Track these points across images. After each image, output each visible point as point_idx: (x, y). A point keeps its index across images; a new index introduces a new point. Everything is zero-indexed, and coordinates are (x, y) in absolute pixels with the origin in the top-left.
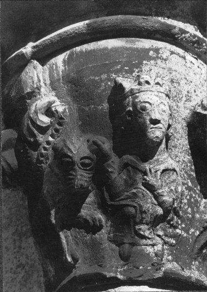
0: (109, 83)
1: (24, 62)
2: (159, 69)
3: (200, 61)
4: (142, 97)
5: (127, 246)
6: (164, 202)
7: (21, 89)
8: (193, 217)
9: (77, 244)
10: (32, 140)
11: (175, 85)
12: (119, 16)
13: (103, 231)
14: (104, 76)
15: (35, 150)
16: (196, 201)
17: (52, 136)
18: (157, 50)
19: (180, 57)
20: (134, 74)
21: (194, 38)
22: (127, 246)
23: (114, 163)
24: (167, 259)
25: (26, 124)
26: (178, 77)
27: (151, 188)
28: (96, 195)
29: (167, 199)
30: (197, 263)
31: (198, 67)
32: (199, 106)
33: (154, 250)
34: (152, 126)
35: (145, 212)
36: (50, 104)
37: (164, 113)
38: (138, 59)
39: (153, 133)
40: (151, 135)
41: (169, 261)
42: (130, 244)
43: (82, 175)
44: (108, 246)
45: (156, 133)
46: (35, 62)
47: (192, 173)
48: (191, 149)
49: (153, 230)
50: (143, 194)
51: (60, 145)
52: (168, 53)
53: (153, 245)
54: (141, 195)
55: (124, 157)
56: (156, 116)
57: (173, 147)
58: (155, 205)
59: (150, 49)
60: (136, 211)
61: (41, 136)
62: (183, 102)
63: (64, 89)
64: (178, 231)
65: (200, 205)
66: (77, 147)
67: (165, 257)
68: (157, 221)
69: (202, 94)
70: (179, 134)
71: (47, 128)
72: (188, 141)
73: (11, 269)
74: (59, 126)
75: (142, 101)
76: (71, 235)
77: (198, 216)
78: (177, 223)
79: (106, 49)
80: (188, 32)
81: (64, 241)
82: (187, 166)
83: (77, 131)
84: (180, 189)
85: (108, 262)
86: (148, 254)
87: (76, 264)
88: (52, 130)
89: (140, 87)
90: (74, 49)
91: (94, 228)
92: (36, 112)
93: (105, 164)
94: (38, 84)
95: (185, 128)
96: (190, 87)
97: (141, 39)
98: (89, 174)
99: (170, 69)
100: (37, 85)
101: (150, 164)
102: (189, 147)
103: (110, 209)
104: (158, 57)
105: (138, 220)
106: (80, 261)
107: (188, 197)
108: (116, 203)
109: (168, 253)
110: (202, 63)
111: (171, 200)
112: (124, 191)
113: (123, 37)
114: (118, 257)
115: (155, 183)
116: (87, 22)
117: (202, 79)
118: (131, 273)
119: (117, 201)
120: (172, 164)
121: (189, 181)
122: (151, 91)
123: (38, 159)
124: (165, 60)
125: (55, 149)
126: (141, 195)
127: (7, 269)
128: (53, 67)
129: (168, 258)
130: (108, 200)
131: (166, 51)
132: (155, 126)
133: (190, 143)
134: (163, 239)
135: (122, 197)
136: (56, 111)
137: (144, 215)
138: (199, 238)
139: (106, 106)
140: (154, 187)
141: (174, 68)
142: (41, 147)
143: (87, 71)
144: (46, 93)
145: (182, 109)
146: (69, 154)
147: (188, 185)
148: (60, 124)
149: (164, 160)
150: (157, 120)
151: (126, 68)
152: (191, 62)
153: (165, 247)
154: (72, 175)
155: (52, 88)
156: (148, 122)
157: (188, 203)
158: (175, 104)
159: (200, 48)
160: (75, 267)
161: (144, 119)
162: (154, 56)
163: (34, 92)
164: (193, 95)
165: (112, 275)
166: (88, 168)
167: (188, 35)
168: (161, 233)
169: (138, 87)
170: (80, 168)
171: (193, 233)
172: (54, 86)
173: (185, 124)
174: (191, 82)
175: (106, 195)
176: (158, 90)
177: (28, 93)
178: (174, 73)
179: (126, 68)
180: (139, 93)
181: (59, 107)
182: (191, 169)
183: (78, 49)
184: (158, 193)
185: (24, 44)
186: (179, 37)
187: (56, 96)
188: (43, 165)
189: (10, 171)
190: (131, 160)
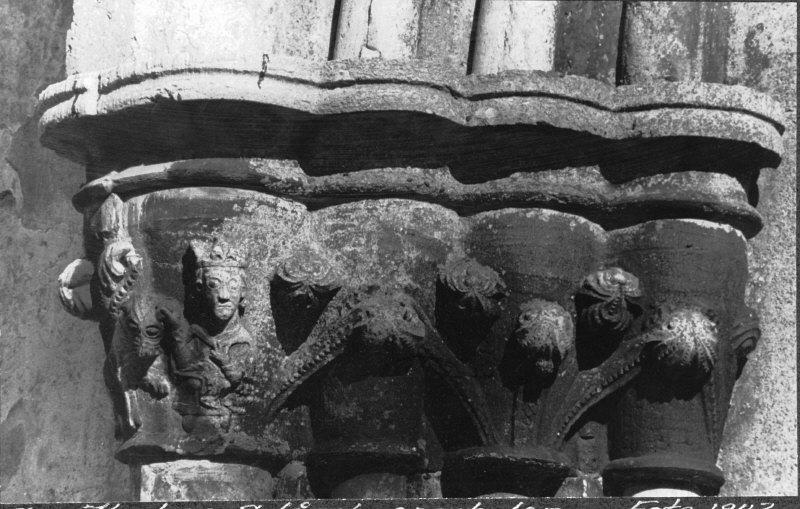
1: (102, 195)
7: (100, 225)
9: (141, 406)
13: (168, 397)
14: (181, 233)
15: (109, 296)
17: (125, 287)
18: (242, 203)
22: (191, 417)
23: (184, 329)
27: (219, 363)
36: (126, 252)
38: (212, 219)
44: (173, 415)
45: (224, 311)
46: (116, 197)
53: (219, 416)
56: (225, 294)
59: (234, 202)
63: (141, 237)
64: (250, 398)
67: (232, 427)
68: (222, 393)
71: (121, 277)
79: (187, 199)
81: (128, 401)
91: (158, 393)
97: (228, 189)
101: (218, 338)
104: (242, 212)
111: (240, 373)
113: (202, 185)
116: (168, 165)
118: (462, 64)
123: (110, 308)
124: (251, 214)
133: (272, 304)
135: (188, 369)
137: (210, 388)
148: (133, 277)
149: (240, 332)
153: (233, 416)
156: (216, 300)
161: (213, 296)
165: (172, 448)
167: (279, 184)
168: (228, 403)
173: (267, 283)
175: (173, 362)
181: (134, 258)
183: (159, 193)
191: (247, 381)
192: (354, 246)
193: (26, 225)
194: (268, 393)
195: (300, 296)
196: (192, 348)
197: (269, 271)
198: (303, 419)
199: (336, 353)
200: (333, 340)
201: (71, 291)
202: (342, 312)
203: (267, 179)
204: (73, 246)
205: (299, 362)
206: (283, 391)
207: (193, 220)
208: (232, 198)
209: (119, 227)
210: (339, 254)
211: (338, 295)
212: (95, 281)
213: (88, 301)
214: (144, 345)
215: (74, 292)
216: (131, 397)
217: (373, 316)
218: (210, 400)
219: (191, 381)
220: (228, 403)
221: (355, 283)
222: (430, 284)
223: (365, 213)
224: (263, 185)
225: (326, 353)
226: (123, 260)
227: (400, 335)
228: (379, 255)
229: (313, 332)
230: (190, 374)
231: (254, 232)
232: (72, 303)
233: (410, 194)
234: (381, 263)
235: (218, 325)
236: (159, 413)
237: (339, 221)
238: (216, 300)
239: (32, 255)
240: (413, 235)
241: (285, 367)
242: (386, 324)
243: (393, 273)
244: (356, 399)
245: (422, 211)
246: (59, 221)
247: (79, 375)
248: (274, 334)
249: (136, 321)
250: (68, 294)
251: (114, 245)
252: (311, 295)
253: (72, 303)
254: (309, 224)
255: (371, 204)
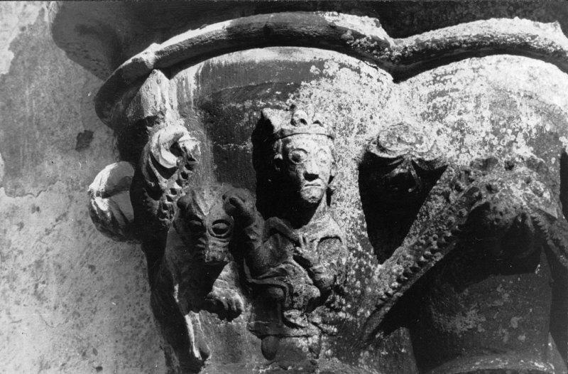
0: (255, 114)
1: (142, 73)
2: (323, 92)
3: (381, 71)
4: (296, 142)
5: (272, 339)
6: (321, 281)
7: (140, 111)
8: (363, 292)
9: (207, 333)
10: (153, 184)
11: (344, 112)
12: (272, 15)
13: (242, 316)
14: (248, 104)
15: (157, 199)
16: (369, 270)
17: (179, 182)
18: (320, 64)
19: (352, 70)
20: (288, 102)
21: (372, 43)
22: (272, 339)
23: (258, 226)
24: (325, 354)
25: (145, 162)
26: (348, 101)
27: (305, 263)
28: (233, 269)
29: (326, 276)
30: (367, 353)
31: (378, 80)
32: (374, 143)
33: (308, 343)
34: (307, 182)
35: (296, 295)
36: (178, 136)
37: (323, 164)
38: (288, 83)
39: (308, 193)
40: (306, 195)
41: (327, 357)
42: (275, 336)
43: (214, 244)
44: (248, 337)
45: (312, 191)
47: (363, 233)
48: (362, 199)
49: (308, 316)
50: (294, 271)
51: (188, 200)
52: (336, 66)
53: (307, 337)
54: (291, 271)
55: (272, 219)
56: (312, 169)
57: (338, 200)
58: (310, 284)
59: (311, 64)
60: (285, 293)
61: (164, 180)
62: (354, 135)
63: (197, 116)
64: (341, 315)
65: (373, 274)
66: (209, 206)
67: (323, 351)
68: (310, 305)
69: (381, 119)
70: (348, 180)
71: (173, 170)
72: (358, 190)
73: (132, 319)
74: (189, 169)
75: (295, 148)
76: (201, 320)
77: (369, 290)
78: (340, 304)
79: (252, 63)
80: (364, 36)
82: (357, 224)
83: (210, 179)
84: (344, 261)
85: (247, 360)
86: (300, 349)
87: (205, 360)
88: (179, 175)
89: (293, 127)
90: (211, 60)
91: (229, 312)
92: (158, 147)
93: (246, 229)
94: (162, 107)
95: (355, 171)
96: (365, 112)
97: (301, 48)
98: (225, 242)
99: (338, 91)
100: (160, 108)
101: (305, 231)
102: (359, 197)
103: (251, 289)
104: (321, 75)
105: (287, 305)
106: (210, 357)
107: (357, 267)
108: (261, 282)
109: (326, 346)
110: (384, 72)
111: (332, 277)
112: (269, 266)
114: (261, 354)
115: (310, 257)
116: (227, 23)
117: (382, 97)
119: (260, 279)
120: (333, 230)
121: (359, 244)
122: (307, 133)
123: (159, 211)
124: (332, 78)
125: (181, 205)
126: (291, 271)
127: (127, 320)
128: (182, 84)
129: (326, 353)
130: (249, 276)
131: (333, 63)
132: (311, 183)
134: (320, 328)
135: (267, 275)
136: (185, 148)
137: (295, 299)
138: (371, 321)
139: (249, 145)
140: (309, 262)
141: (343, 89)
142: (164, 195)
143: (227, 95)
144: (171, 119)
145: (352, 145)
146: (198, 216)
147: (357, 250)
148: (189, 167)
150: (313, 175)
151: (277, 92)
152: (369, 75)
154: (201, 243)
155: (180, 113)
156: (302, 177)
157: (356, 274)
158: (342, 139)
159: (381, 55)
160: (203, 365)
161: (297, 172)
162: (317, 73)
163: (156, 117)
164: (369, 124)
166: (223, 235)
167: (363, 40)
168: (318, 320)
169: (290, 127)
170: (212, 235)
171: (363, 314)
172: (182, 111)
173: (355, 166)
174: (367, 105)
175: (247, 270)
176: (317, 132)
177: (148, 118)
178: (343, 96)
179: (277, 92)
180: (291, 135)
181: (189, 143)
182: (362, 227)
183: (215, 60)
184: (314, 270)
185: (143, 46)
186: (351, 44)
187: (186, 125)
188: (166, 219)
189: (123, 223)
190: (280, 225)
191: (338, 290)
192: (460, 114)
193: (10, 194)
194: (362, 310)
195: (400, 174)
196: (271, 247)
197: (357, 151)
198: (404, 344)
199: (448, 250)
200: (440, 233)
201: (106, 200)
202: (451, 197)
203: (348, 34)
204: (74, 205)
205: (397, 268)
206: (379, 307)
207: (264, 86)
208: (308, 60)
209: (166, 110)
210: (441, 126)
211: (443, 178)
212: (140, 184)
213: (129, 210)
214: (210, 247)
215: (110, 202)
216: (193, 322)
217: (497, 191)
218: (295, 316)
219: (271, 291)
220: (318, 320)
221: (464, 160)
222: (553, 160)
223: (471, 74)
224: (344, 41)
225: (433, 251)
226: (175, 148)
227: (531, 214)
228: (492, 122)
229: (411, 232)
230: (268, 281)
231: (337, 101)
232: (109, 214)
233: (522, 48)
234: (496, 132)
235: (304, 212)
236: (231, 338)
237: (439, 87)
238: (302, 177)
239: (21, 226)
240: (531, 97)
241: (379, 277)
242: (515, 200)
243: (510, 144)
244: (473, 306)
245: (538, 71)
246: (53, 181)
247: (95, 352)
248: (365, 234)
249: (200, 216)
250: (103, 204)
251: (161, 132)
252: (413, 173)
253: (109, 214)
254: (398, 97)
255: (476, 62)
